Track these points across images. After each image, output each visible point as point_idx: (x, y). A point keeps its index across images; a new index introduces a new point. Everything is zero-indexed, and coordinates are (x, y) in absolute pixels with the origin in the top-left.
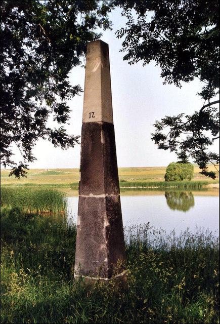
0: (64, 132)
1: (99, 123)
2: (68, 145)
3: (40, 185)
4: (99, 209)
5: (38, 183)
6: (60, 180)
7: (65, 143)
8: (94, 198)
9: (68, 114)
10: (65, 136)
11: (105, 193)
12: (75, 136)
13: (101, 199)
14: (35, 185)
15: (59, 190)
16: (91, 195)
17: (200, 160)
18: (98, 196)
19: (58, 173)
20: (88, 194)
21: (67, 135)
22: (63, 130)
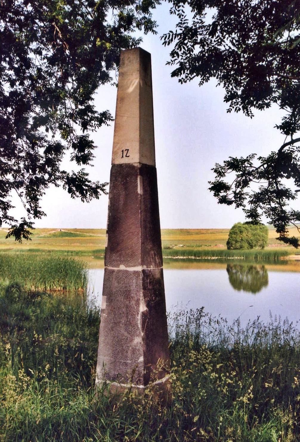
0: (86, 177)
1: (136, 165)
2: (91, 195)
3: (49, 251)
5: (46, 248)
9: (92, 151)
10: (87, 183)
11: (142, 264)
13: (136, 273)
15: (77, 258)
16: (122, 267)
18: (131, 269)
19: (76, 235)
20: (118, 266)
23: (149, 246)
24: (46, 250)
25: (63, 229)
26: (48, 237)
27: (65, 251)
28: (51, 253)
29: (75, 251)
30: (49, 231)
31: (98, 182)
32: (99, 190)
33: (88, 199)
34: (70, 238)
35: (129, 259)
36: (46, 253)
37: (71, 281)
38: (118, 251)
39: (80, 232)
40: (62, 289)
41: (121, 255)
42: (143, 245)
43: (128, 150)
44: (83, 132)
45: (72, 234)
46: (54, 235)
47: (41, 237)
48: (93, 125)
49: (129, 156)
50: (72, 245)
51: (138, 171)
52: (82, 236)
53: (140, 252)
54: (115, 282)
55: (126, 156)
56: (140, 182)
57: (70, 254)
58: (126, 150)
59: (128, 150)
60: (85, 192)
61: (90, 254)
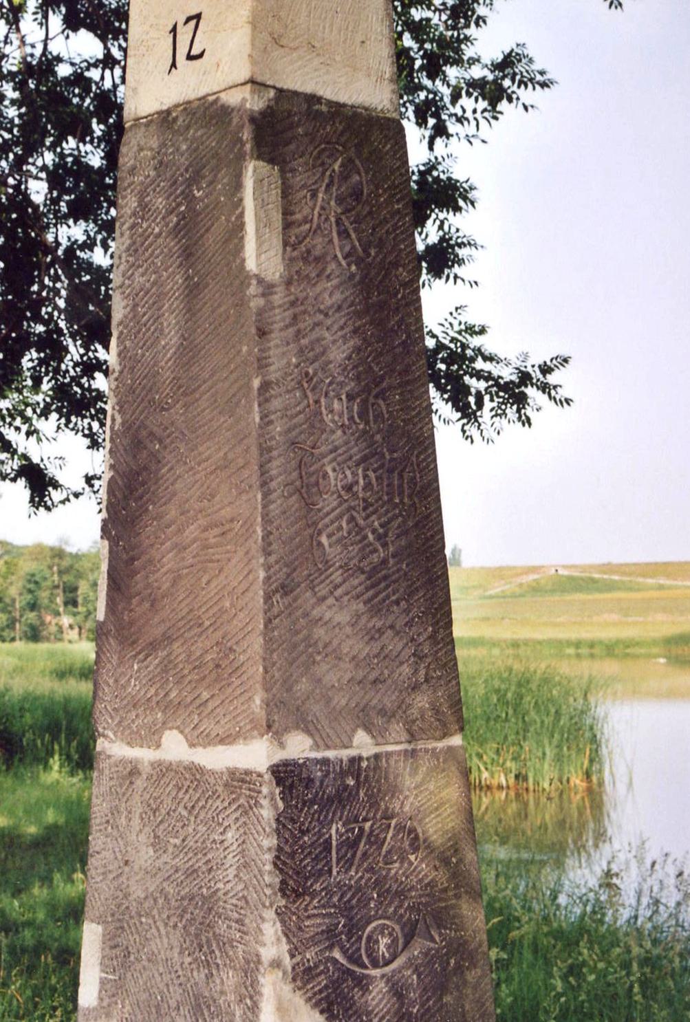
0: (475, 341)
1: (232, 99)
2: (499, 413)
3: (515, 644)
4: (228, 880)
5: (506, 633)
6: (615, 617)
7: (480, 404)
8: (196, 771)
9: (455, 221)
10: (480, 364)
11: (273, 729)
12: (537, 358)
13: (240, 780)
14: (494, 643)
15: (565, 668)
16: (174, 747)
17: (459, 41)
18: (217, 759)
19: (610, 587)
20: (152, 737)
21: (489, 358)
22: (471, 330)
23: (338, 616)
24: (505, 641)
25: (564, 567)
26: (514, 596)
27: (569, 643)
28: (521, 651)
29: (601, 642)
30: (517, 575)
31: (526, 356)
32: (531, 391)
33: (489, 432)
34: (590, 597)
35: (205, 695)
36: (502, 650)
37: (540, 754)
38: (153, 646)
39: (624, 574)
40: (512, 781)
41: (165, 670)
42: (279, 601)
43: (198, 17)
44: (431, 148)
45: (593, 580)
46: (536, 589)
47: (491, 597)
48: (469, 114)
49: (201, 56)
50: (595, 619)
51: (247, 135)
52: (630, 589)
53: (256, 644)
54: (142, 838)
55: (190, 57)
56: (261, 204)
57: (584, 651)
58: (189, 20)
59: (198, 17)
60: (472, 400)
61: (655, 650)
